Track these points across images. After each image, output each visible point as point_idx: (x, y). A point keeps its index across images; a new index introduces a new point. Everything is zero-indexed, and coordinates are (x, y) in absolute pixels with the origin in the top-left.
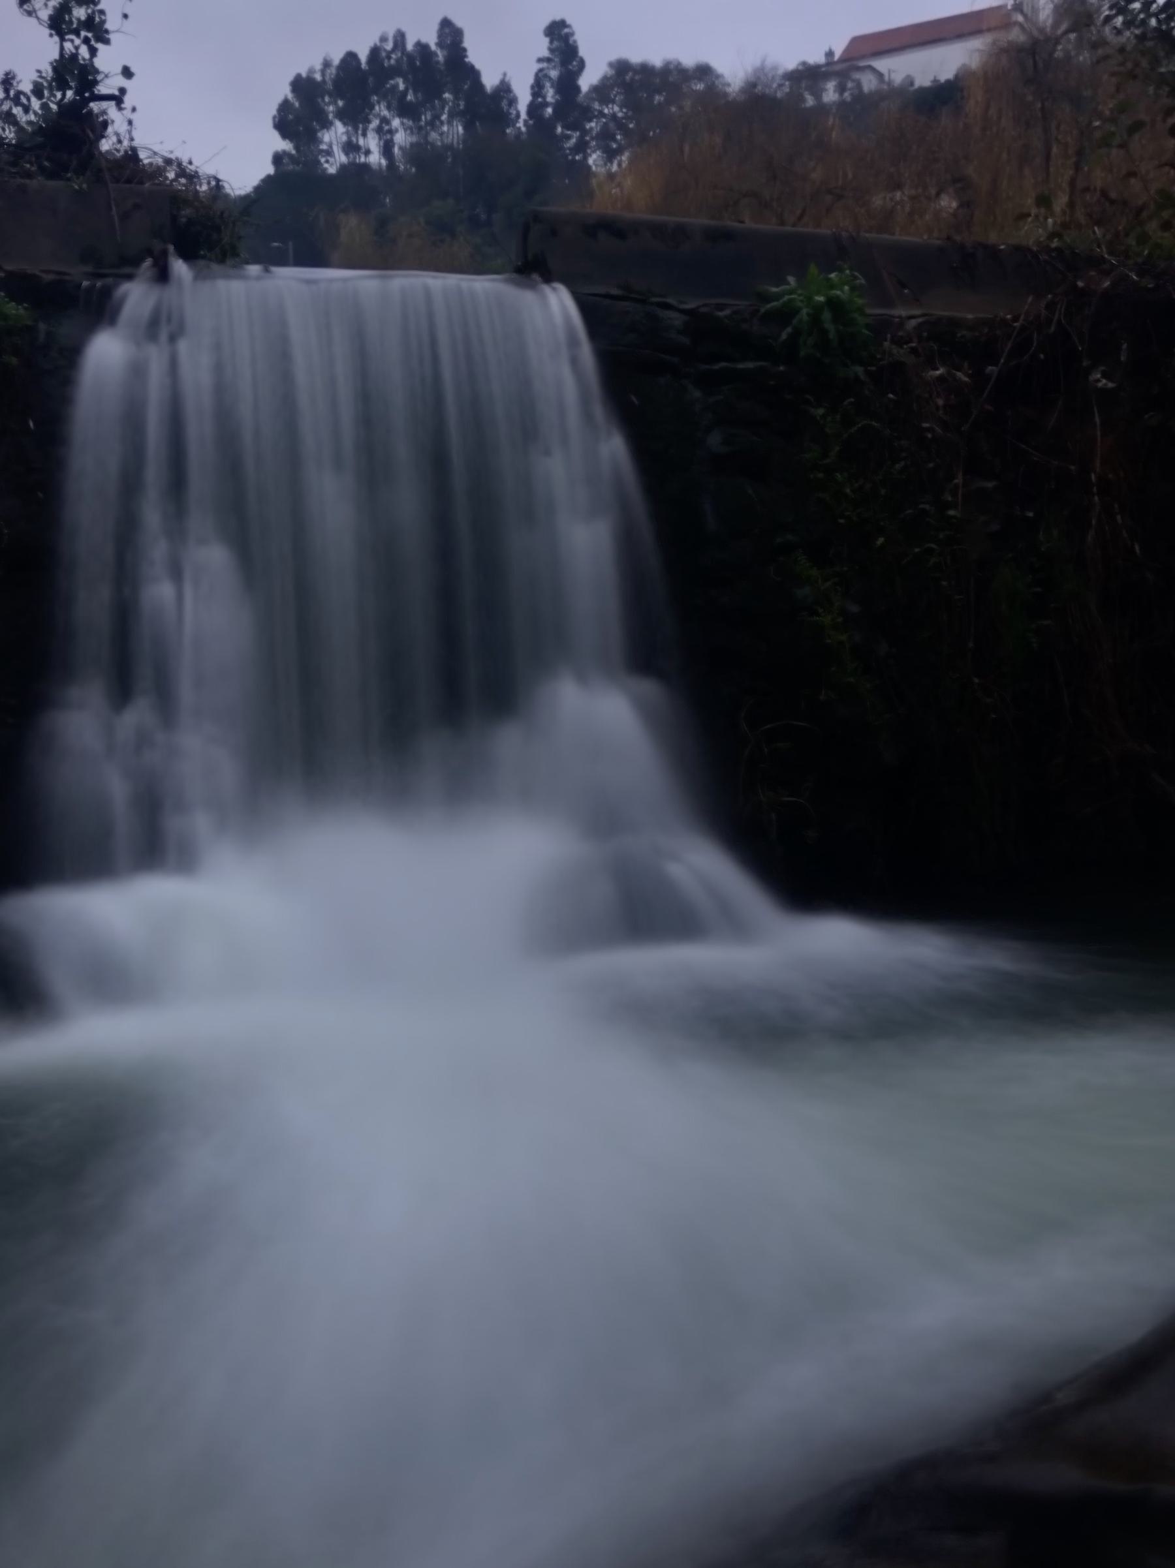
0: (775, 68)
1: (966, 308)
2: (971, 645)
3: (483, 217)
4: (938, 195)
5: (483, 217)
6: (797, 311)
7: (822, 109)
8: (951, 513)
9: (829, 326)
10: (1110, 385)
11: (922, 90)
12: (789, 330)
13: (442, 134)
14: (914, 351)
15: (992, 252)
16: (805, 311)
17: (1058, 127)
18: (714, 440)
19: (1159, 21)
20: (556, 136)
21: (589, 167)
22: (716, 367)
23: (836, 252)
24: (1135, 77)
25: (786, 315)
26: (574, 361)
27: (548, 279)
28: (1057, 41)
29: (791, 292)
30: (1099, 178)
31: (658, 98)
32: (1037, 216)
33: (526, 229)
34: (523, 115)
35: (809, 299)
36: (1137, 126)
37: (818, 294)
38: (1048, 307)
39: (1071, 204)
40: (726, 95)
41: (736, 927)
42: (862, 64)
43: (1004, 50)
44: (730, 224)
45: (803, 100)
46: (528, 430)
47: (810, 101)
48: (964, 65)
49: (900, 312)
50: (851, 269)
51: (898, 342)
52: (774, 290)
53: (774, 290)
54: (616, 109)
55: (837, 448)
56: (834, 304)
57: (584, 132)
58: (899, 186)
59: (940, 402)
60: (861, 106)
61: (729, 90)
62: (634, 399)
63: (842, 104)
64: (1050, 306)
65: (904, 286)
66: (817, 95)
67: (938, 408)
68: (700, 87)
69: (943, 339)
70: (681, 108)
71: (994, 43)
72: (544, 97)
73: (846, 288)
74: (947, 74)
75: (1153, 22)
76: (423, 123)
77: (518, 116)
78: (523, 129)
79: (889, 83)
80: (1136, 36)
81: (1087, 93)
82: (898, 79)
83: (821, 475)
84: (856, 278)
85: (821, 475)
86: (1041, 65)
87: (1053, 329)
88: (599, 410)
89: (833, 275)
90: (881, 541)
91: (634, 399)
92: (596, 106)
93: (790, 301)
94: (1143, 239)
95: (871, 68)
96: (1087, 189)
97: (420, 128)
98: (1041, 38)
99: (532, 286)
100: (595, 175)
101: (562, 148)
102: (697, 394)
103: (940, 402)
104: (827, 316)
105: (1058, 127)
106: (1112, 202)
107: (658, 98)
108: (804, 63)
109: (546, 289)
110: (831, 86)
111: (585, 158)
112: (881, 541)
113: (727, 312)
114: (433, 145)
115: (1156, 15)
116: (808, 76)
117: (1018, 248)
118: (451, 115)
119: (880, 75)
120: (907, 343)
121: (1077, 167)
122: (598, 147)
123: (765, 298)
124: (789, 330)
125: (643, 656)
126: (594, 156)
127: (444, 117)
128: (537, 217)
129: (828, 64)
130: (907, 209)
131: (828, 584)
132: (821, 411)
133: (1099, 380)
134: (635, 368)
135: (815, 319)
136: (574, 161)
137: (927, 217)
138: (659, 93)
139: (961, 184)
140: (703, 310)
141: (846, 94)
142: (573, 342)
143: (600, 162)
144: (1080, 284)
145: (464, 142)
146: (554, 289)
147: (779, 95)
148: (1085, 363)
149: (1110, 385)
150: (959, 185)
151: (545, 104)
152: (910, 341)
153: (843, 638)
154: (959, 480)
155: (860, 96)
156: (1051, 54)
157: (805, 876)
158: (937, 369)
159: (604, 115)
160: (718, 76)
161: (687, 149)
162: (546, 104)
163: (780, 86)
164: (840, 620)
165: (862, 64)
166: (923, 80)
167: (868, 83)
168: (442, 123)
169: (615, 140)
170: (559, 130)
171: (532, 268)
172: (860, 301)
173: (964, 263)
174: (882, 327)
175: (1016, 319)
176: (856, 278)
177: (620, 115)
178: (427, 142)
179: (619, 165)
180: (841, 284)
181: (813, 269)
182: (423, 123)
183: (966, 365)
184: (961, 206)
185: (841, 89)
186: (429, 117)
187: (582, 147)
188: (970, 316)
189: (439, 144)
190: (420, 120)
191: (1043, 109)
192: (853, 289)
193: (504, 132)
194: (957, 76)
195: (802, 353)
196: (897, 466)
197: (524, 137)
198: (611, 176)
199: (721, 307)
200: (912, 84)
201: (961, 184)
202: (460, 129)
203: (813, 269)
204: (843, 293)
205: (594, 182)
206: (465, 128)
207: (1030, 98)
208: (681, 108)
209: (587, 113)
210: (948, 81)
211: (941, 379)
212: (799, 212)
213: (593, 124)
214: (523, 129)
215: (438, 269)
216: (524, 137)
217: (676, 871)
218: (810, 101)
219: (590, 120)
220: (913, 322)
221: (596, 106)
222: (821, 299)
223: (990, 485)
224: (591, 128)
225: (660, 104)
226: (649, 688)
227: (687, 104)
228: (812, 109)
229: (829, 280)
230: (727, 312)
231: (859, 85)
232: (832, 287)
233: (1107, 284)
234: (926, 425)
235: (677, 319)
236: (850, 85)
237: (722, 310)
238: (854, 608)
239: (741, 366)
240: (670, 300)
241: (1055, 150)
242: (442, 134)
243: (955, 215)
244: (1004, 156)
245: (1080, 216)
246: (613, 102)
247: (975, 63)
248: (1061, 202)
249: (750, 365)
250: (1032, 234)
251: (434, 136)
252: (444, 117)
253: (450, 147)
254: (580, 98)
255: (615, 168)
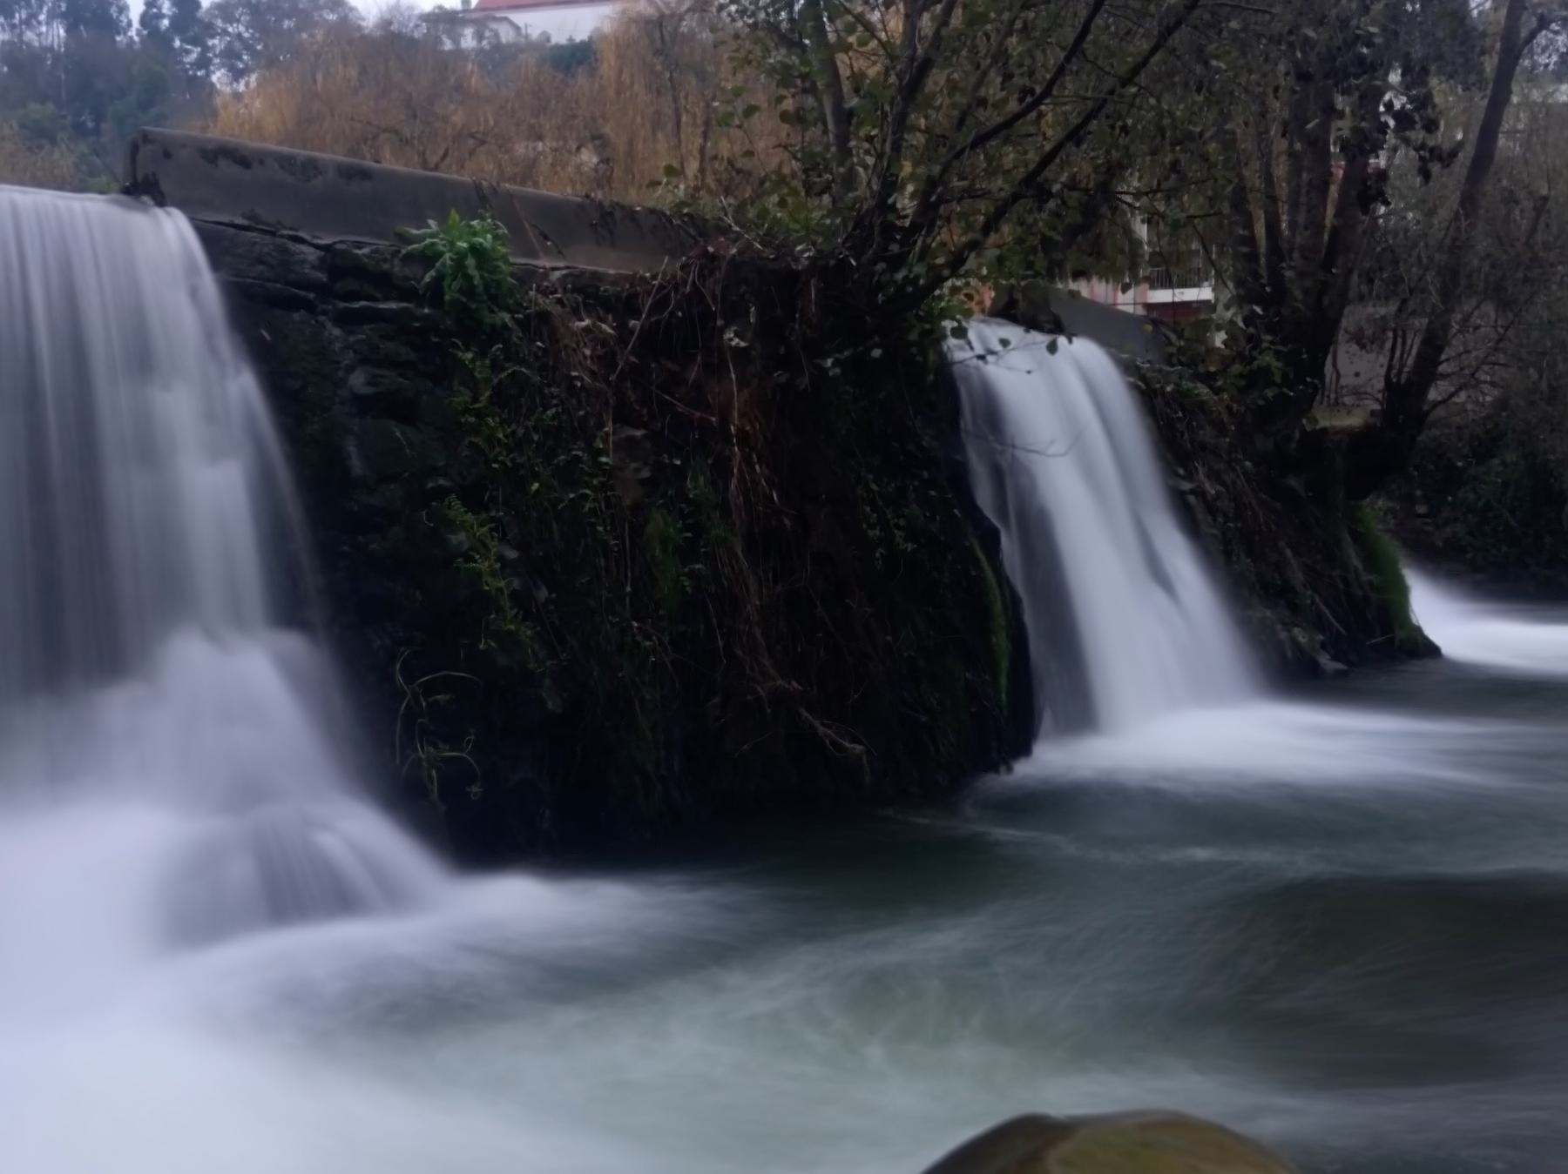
0: (411, 8)
1: (610, 265)
2: (628, 589)
3: (90, 125)
4: (578, 149)
5: (90, 125)
6: (441, 254)
7: (459, 54)
8: (604, 459)
9: (472, 271)
10: (743, 344)
11: (558, 47)
12: (432, 273)
13: (39, 35)
14: (559, 301)
15: (630, 214)
16: (447, 255)
17: (686, 97)
18: (358, 381)
19: (767, 14)
20: (173, 49)
21: (212, 85)
22: (357, 305)
23: (478, 200)
24: (750, 63)
25: (428, 258)
26: (194, 293)
27: (161, 202)
28: (681, 19)
29: (432, 236)
30: (725, 149)
31: (287, 24)
32: (668, 183)
33: (135, 149)
34: (136, 24)
35: (452, 244)
36: (751, 110)
37: (460, 239)
38: (682, 268)
39: (702, 170)
40: (360, 28)
41: (395, 896)
42: (499, 15)
43: (631, 21)
44: (369, 163)
45: (441, 42)
46: (142, 360)
47: (448, 45)
48: (597, 29)
49: (544, 262)
50: (493, 217)
51: (545, 292)
52: (415, 232)
53: (415, 232)
54: (242, 28)
55: (488, 394)
56: (475, 250)
57: (206, 49)
58: (540, 138)
59: (588, 352)
60: (499, 57)
61: (364, 24)
62: (265, 334)
63: (481, 51)
64: (684, 267)
65: (546, 238)
66: (456, 40)
67: (585, 357)
68: (332, 17)
69: (588, 293)
70: (312, 36)
71: (624, 12)
72: (159, 8)
73: (489, 236)
74: (581, 35)
75: (762, 15)
76: (16, 21)
77: (130, 24)
78: (136, 39)
79: (527, 36)
80: (749, 26)
81: (710, 69)
82: (535, 34)
83: (472, 419)
84: (498, 227)
85: (472, 419)
86: (667, 37)
87: (688, 289)
88: (226, 344)
89: (474, 223)
90: (536, 485)
91: (265, 334)
92: (219, 23)
93: (433, 244)
94: (763, 214)
95: (506, 19)
96: (715, 158)
97: (13, 27)
98: (668, 12)
99: (144, 208)
100: (218, 92)
101: (181, 62)
102: (337, 332)
103: (588, 352)
104: (471, 262)
105: (686, 97)
106: (739, 171)
107: (287, 24)
108: (440, 7)
109: (159, 212)
110: (469, 32)
111: (208, 75)
112: (536, 485)
113: (366, 250)
114: (29, 45)
115: (765, 8)
116: (444, 20)
117: (652, 211)
118: (52, 16)
119: (517, 28)
120: (552, 293)
121: (705, 136)
122: (223, 65)
123: (406, 239)
124: (432, 273)
125: (288, 610)
126: (218, 74)
127: (42, 17)
128: (146, 138)
129: (464, 11)
130: (550, 160)
131: (485, 529)
132: (470, 355)
133: (732, 338)
134: (270, 303)
135: (460, 258)
136: (195, 76)
137: (570, 169)
138: (289, 18)
139: (600, 141)
140: (339, 246)
141: (485, 42)
142: (192, 269)
143: (225, 80)
144: (711, 249)
145: (66, 45)
146: (168, 214)
147: (416, 35)
148: (720, 323)
149: (743, 344)
150: (598, 142)
151: (160, 16)
152: (555, 292)
153: (502, 584)
154: (609, 428)
155: (498, 47)
156: (676, 29)
157: (476, 833)
158: (582, 320)
159: (228, 34)
160: (352, 9)
161: (320, 77)
162: (162, 16)
163: (417, 26)
164: (498, 566)
165: (499, 15)
166: (559, 38)
167: (506, 35)
168: (39, 23)
169: (240, 59)
170: (177, 43)
171: (143, 188)
172: (504, 250)
173: (605, 222)
174: (527, 276)
175: (654, 277)
176: (498, 227)
177: (246, 35)
178: (22, 41)
179: (247, 84)
180: (485, 233)
181: (454, 216)
182: (16, 21)
183: (610, 317)
184: (601, 161)
185: (479, 36)
186: (24, 16)
187: (203, 62)
188: (612, 272)
189: (37, 44)
190: (13, 17)
191: (671, 79)
192: (496, 237)
193: (114, 41)
194: (590, 38)
195: (447, 297)
196: (549, 413)
197: (137, 47)
198: (237, 96)
199: (359, 245)
200: (548, 39)
201: (600, 141)
202: (62, 32)
203: (454, 216)
204: (487, 241)
205: (218, 101)
206: (67, 31)
207: (659, 68)
208: (312, 36)
209: (209, 30)
210: (583, 43)
211: (587, 330)
212: (441, 152)
213: (216, 41)
214: (136, 39)
215: (21, 183)
216: (137, 47)
217: (329, 843)
218: (448, 45)
219: (212, 37)
220: (557, 274)
221: (219, 23)
222: (465, 245)
223: (639, 433)
224: (214, 46)
225: (289, 29)
226: (293, 643)
227: (319, 34)
228: (450, 52)
229: (471, 226)
230: (366, 250)
231: (497, 35)
232: (475, 234)
233: (734, 251)
234: (574, 374)
235: (312, 255)
236: (487, 34)
237: (360, 248)
238: (512, 554)
239: (382, 306)
240: (301, 234)
241: (684, 119)
242: (39, 35)
243: (596, 170)
244: (639, 119)
245: (710, 181)
246: (238, 21)
247: (607, 28)
248: (692, 167)
249: (393, 305)
250: (664, 198)
251: (29, 36)
252: (42, 17)
253: (50, 49)
254: (201, 14)
255: (241, 87)
